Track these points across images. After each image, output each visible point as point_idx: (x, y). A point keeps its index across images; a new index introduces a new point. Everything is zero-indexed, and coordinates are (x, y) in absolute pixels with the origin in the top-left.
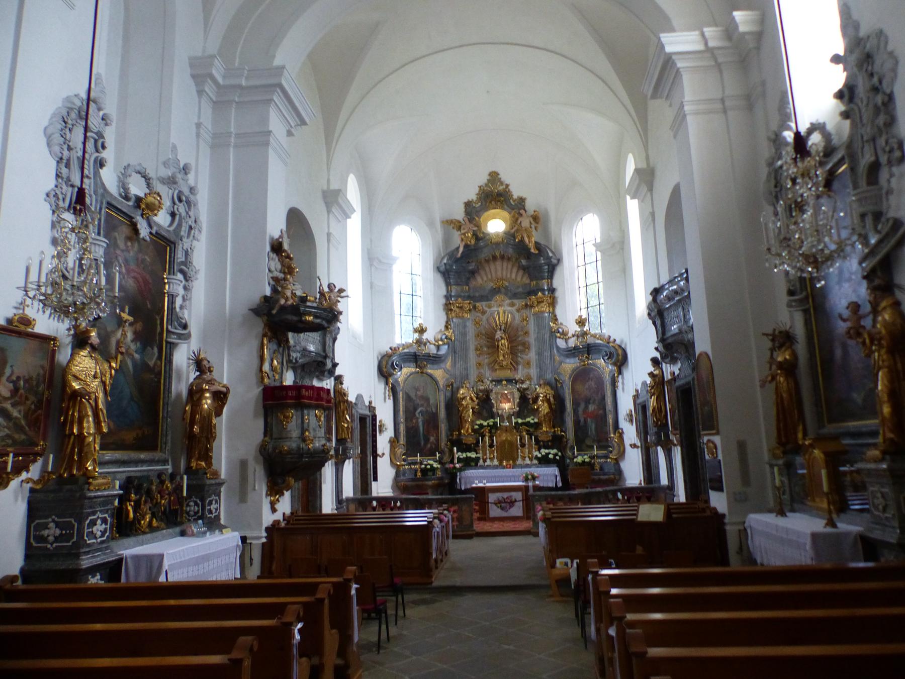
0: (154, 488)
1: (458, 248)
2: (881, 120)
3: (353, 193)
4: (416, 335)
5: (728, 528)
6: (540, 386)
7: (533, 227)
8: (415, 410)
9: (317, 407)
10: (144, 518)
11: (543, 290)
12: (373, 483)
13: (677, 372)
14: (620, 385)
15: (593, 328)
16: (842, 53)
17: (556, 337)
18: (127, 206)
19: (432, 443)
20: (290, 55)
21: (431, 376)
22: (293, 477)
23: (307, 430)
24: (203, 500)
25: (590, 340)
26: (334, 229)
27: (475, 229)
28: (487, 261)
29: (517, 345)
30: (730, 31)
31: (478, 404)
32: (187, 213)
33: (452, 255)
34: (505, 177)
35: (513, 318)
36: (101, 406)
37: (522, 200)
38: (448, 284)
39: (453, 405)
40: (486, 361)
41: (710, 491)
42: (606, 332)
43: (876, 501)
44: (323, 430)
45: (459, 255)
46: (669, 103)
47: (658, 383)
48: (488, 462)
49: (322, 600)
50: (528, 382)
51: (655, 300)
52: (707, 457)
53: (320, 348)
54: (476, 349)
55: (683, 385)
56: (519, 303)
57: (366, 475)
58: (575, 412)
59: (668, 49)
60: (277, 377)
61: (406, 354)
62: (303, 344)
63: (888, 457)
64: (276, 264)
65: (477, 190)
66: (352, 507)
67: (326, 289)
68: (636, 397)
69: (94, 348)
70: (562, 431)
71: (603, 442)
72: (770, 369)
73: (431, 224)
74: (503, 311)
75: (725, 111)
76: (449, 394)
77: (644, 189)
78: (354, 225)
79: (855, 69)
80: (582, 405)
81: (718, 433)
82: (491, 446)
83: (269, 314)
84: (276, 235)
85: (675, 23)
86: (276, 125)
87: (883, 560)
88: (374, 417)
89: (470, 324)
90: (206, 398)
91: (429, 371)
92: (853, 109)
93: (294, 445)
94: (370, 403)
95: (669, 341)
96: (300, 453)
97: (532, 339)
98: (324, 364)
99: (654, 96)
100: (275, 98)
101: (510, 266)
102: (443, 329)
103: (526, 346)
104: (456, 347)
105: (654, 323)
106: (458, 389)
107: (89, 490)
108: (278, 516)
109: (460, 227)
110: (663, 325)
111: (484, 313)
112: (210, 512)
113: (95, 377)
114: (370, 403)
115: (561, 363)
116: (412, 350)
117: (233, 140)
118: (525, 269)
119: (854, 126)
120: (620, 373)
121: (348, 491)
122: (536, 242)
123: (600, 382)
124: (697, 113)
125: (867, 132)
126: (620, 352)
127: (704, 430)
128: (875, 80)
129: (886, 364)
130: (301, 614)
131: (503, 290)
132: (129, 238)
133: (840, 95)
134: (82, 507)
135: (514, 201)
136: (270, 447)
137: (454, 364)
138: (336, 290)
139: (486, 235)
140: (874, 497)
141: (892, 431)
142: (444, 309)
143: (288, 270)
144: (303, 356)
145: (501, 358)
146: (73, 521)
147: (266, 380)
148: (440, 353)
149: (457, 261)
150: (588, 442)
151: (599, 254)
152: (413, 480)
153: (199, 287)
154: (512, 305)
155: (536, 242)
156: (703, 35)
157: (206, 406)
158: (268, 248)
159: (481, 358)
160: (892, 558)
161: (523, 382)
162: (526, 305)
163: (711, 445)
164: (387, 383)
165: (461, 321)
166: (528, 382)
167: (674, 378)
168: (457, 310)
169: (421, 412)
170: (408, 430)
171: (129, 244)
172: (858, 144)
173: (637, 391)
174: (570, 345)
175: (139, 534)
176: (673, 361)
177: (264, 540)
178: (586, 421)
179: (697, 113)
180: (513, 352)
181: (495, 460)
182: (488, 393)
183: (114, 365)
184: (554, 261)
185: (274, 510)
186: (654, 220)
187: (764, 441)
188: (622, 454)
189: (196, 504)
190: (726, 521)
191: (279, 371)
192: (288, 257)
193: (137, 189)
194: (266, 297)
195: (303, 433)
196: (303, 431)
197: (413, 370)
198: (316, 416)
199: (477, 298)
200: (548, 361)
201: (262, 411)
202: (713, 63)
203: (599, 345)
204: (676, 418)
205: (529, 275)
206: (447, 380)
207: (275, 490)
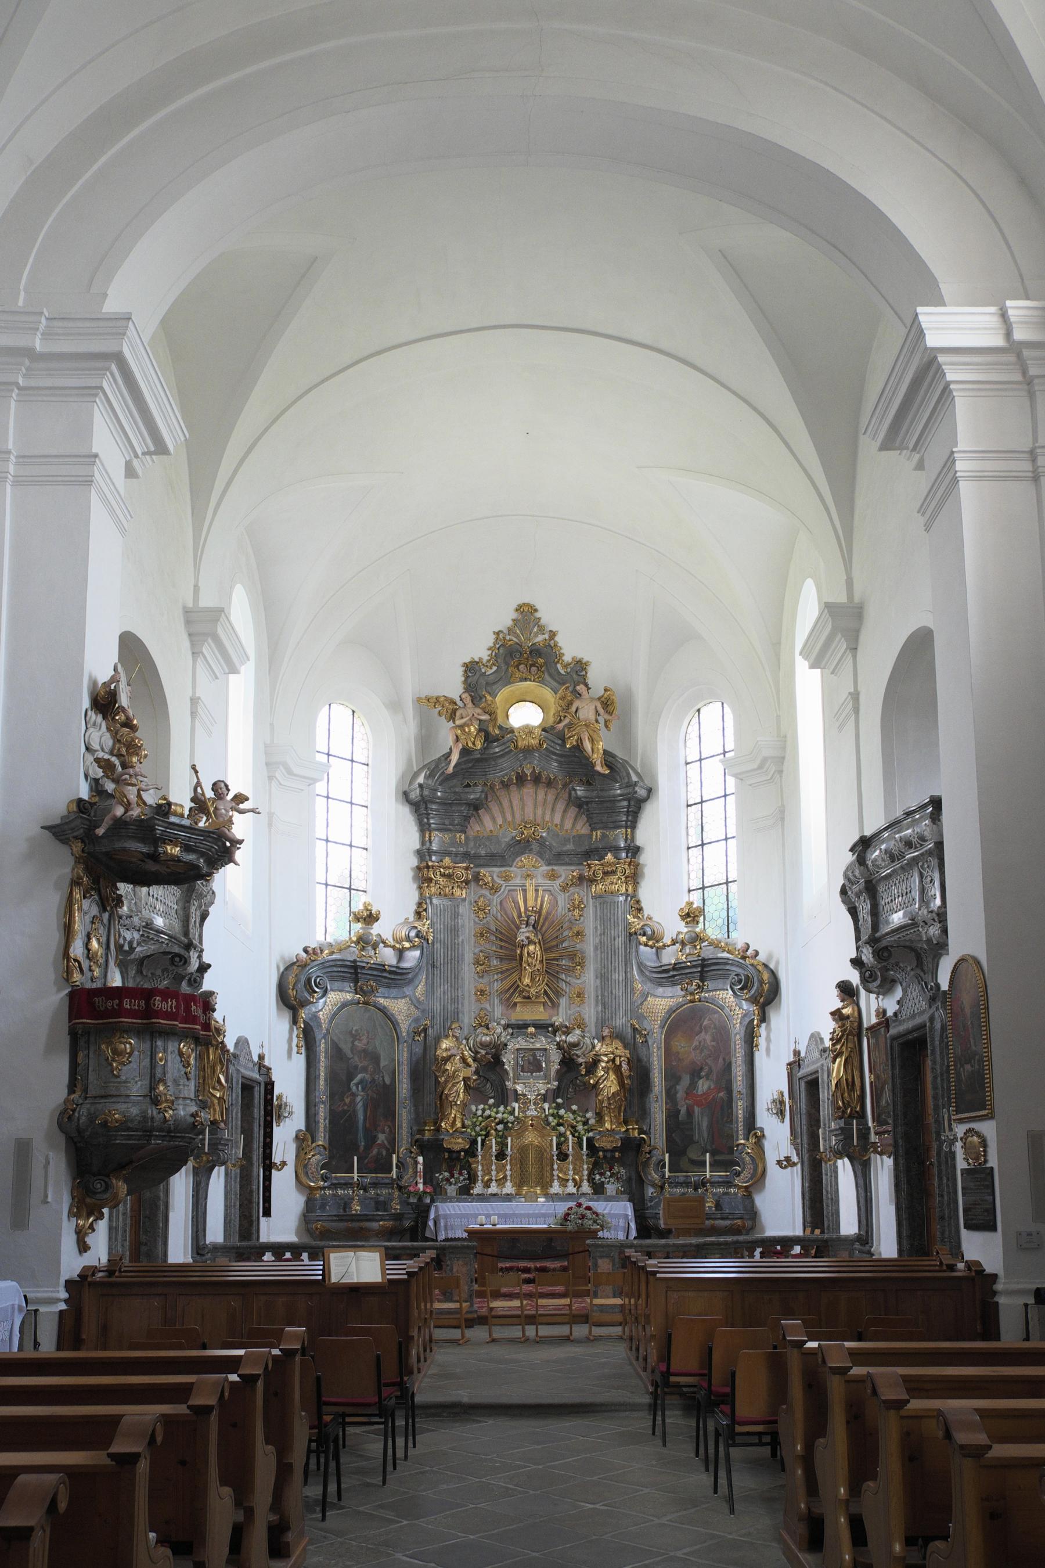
3: (241, 616)
4: (358, 927)
5: (1002, 1300)
6: (603, 1039)
7: (601, 719)
8: (350, 1077)
9: (183, 1036)
11: (615, 850)
12: (263, 1220)
13: (890, 1013)
14: (762, 1041)
15: (712, 929)
19: (382, 1145)
20: (142, 288)
21: (383, 1010)
22: (126, 1180)
23: (162, 1080)
25: (708, 952)
26: (205, 688)
28: (506, 786)
29: (559, 958)
31: (476, 1072)
33: (435, 768)
34: (547, 616)
35: (555, 902)
37: (580, 667)
38: (424, 828)
39: (426, 1072)
40: (496, 986)
41: (964, 1233)
42: (739, 938)
44: (192, 1084)
45: (451, 769)
46: (917, 457)
47: (849, 1030)
48: (494, 1189)
49: (132, 1459)
50: (578, 1032)
51: (861, 861)
53: (177, 926)
54: (477, 963)
55: (909, 1032)
57: (250, 1203)
58: (670, 1094)
59: (932, 340)
60: (97, 973)
61: (335, 963)
62: (145, 913)
64: (101, 737)
65: (490, 641)
67: (209, 794)
71: (726, 1158)
73: (395, 706)
74: (533, 887)
76: (418, 1050)
77: (841, 645)
78: (241, 689)
81: (990, 1117)
82: (501, 1156)
83: (88, 837)
84: (103, 675)
85: (945, 289)
88: (270, 1086)
91: (382, 1001)
93: (134, 1111)
94: (261, 1057)
95: (884, 943)
96: (146, 1129)
97: (589, 946)
98: (186, 961)
99: (885, 447)
100: (105, 385)
101: (551, 797)
102: (411, 919)
103: (577, 960)
104: (437, 953)
105: (853, 912)
106: (438, 1040)
108: (89, 1259)
109: (454, 712)
114: (261, 1057)
115: (645, 996)
117: (12, 469)
118: (580, 805)
120: (763, 1019)
121: (215, 1232)
122: (605, 752)
123: (722, 1035)
124: (979, 477)
126: (766, 976)
127: (957, 1112)
130: (270, 1365)
131: (535, 846)
135: (565, 666)
137: (431, 988)
138: (230, 797)
142: (415, 878)
144: (145, 939)
145: (527, 981)
147: (76, 976)
148: (405, 965)
149: (447, 779)
150: (693, 1154)
151: (731, 781)
152: (341, 1219)
154: (553, 876)
155: (605, 752)
156: (1004, 315)
158: (86, 703)
159: (485, 980)
161: (567, 1033)
162: (581, 878)
164: (295, 1021)
166: (578, 1032)
167: (885, 1021)
168: (442, 881)
169: (361, 1082)
170: (334, 1117)
173: (797, 1053)
176: (885, 987)
177: (63, 1306)
178: (690, 1113)
179: (979, 477)
180: (551, 971)
181: (509, 1184)
184: (641, 792)
185: (83, 1247)
186: (856, 710)
188: (759, 1178)
190: (999, 1287)
191: (101, 961)
192: (128, 724)
194: (80, 801)
195: (152, 1088)
197: (349, 997)
198: (181, 1054)
199: (482, 860)
200: (619, 992)
201: (65, 1040)
202: (1018, 377)
203: (726, 962)
204: (887, 1096)
205: (589, 819)
207: (86, 1203)
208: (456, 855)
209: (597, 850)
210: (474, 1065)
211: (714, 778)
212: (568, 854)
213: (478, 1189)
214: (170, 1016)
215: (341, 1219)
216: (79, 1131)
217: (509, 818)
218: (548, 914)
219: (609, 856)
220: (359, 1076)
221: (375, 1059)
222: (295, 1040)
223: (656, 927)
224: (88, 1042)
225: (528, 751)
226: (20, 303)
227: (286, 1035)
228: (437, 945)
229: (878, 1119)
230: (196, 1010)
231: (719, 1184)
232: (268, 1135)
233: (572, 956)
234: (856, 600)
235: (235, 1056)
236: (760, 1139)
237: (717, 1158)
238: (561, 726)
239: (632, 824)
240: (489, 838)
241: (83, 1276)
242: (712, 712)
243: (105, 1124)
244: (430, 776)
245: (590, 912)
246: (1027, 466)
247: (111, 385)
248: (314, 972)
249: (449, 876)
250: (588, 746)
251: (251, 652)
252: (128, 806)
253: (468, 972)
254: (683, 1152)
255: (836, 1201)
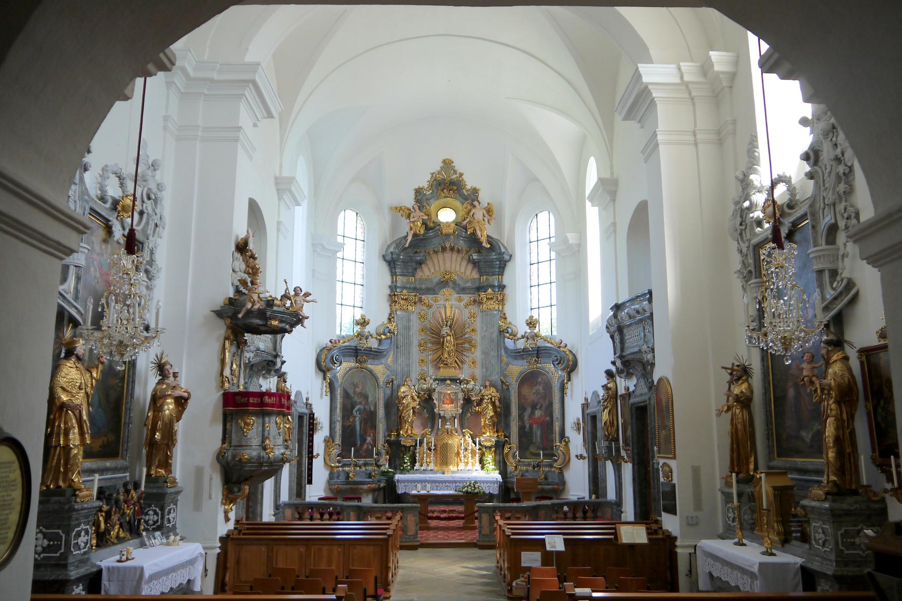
0: (122, 497)
1: (406, 237)
2: (842, 187)
5: (679, 550)
7: (486, 219)
8: (353, 407)
10: (113, 527)
11: (493, 287)
12: (307, 486)
13: (632, 389)
14: (568, 391)
16: (810, 117)
17: (505, 337)
18: (104, 209)
21: (371, 371)
23: (267, 438)
24: (162, 509)
25: (541, 343)
27: (426, 217)
28: (436, 252)
29: (463, 343)
30: (705, 68)
31: (419, 404)
32: (154, 210)
34: (459, 166)
36: (85, 418)
37: (475, 191)
38: (393, 274)
39: (393, 405)
40: (430, 358)
43: (817, 535)
45: (407, 245)
47: (612, 396)
51: (615, 316)
52: (662, 480)
54: (420, 345)
56: (466, 298)
57: (303, 477)
58: (521, 417)
61: (346, 348)
63: (829, 497)
64: (240, 265)
65: (429, 177)
66: (288, 512)
68: (585, 406)
69: (79, 359)
70: (505, 436)
72: (728, 401)
74: (451, 306)
75: (696, 144)
76: (388, 392)
78: (300, 213)
79: (821, 137)
80: (529, 410)
81: (674, 458)
83: (234, 317)
84: (242, 234)
85: (653, 52)
86: (245, 119)
87: (819, 589)
89: (414, 318)
90: (168, 404)
92: (817, 172)
95: (626, 359)
96: (260, 462)
98: (274, 364)
99: (627, 117)
101: (459, 259)
105: (612, 337)
106: (399, 387)
107: (75, 502)
109: (410, 214)
110: (622, 342)
111: (430, 306)
112: (169, 521)
113: (80, 388)
114: (307, 399)
115: (508, 364)
116: (353, 344)
118: (475, 264)
119: (817, 186)
120: (569, 380)
122: (488, 236)
123: (548, 387)
125: (830, 197)
126: (571, 357)
128: (838, 151)
129: (834, 413)
131: (451, 284)
132: (105, 241)
133: (806, 157)
134: (70, 518)
136: (229, 455)
137: (396, 360)
139: (438, 224)
140: (816, 532)
141: (835, 474)
143: (254, 272)
144: (256, 356)
145: (446, 355)
146: (60, 532)
147: (227, 385)
150: (533, 449)
151: (553, 255)
153: (161, 283)
155: (488, 236)
156: (679, 69)
157: (167, 412)
158: (233, 248)
159: (424, 354)
160: (828, 587)
162: (475, 301)
163: (667, 469)
164: (325, 379)
165: (404, 313)
166: (472, 383)
167: (628, 395)
168: (402, 302)
169: (358, 410)
170: (344, 429)
171: (104, 247)
172: (819, 205)
173: (586, 399)
174: (519, 347)
175: (109, 546)
176: (629, 375)
177: (218, 551)
178: (531, 427)
180: (460, 350)
182: (430, 392)
183: (95, 375)
184: (506, 257)
186: (615, 231)
187: (717, 468)
188: (567, 463)
189: (156, 513)
190: (678, 543)
191: (237, 374)
192: (253, 257)
193: (113, 191)
194: (230, 298)
195: (263, 442)
196: (264, 439)
197: (353, 364)
199: (421, 291)
202: (687, 96)
204: (629, 433)
206: (387, 376)
207: (229, 497)
208: (410, 288)
209: (483, 287)
210: (418, 400)
211: (544, 251)
212: (468, 288)
213: (417, 466)
214: (272, 405)
215: (348, 483)
216: (228, 464)
217: (437, 269)
218: (457, 319)
219: (490, 290)
220: (358, 407)
221: (366, 397)
222: (324, 388)
223: (514, 328)
224: (232, 419)
225: (448, 235)
226: (206, 57)
227: (320, 386)
228: (399, 336)
229: (625, 441)
230: (284, 401)
231: (546, 466)
232: (311, 441)
233: (470, 342)
234: (615, 176)
235: (295, 402)
236: (567, 443)
237: (546, 452)
238: (465, 223)
239: (501, 273)
240: (427, 280)
241: (228, 535)
242: (543, 216)
243: (240, 459)
244: (397, 246)
245: (479, 319)
246: (692, 138)
247: (250, 93)
248: (335, 352)
249: (406, 299)
250: (479, 233)
251: (306, 193)
252: (253, 303)
253: (415, 350)
254: (527, 449)
255: (605, 481)
